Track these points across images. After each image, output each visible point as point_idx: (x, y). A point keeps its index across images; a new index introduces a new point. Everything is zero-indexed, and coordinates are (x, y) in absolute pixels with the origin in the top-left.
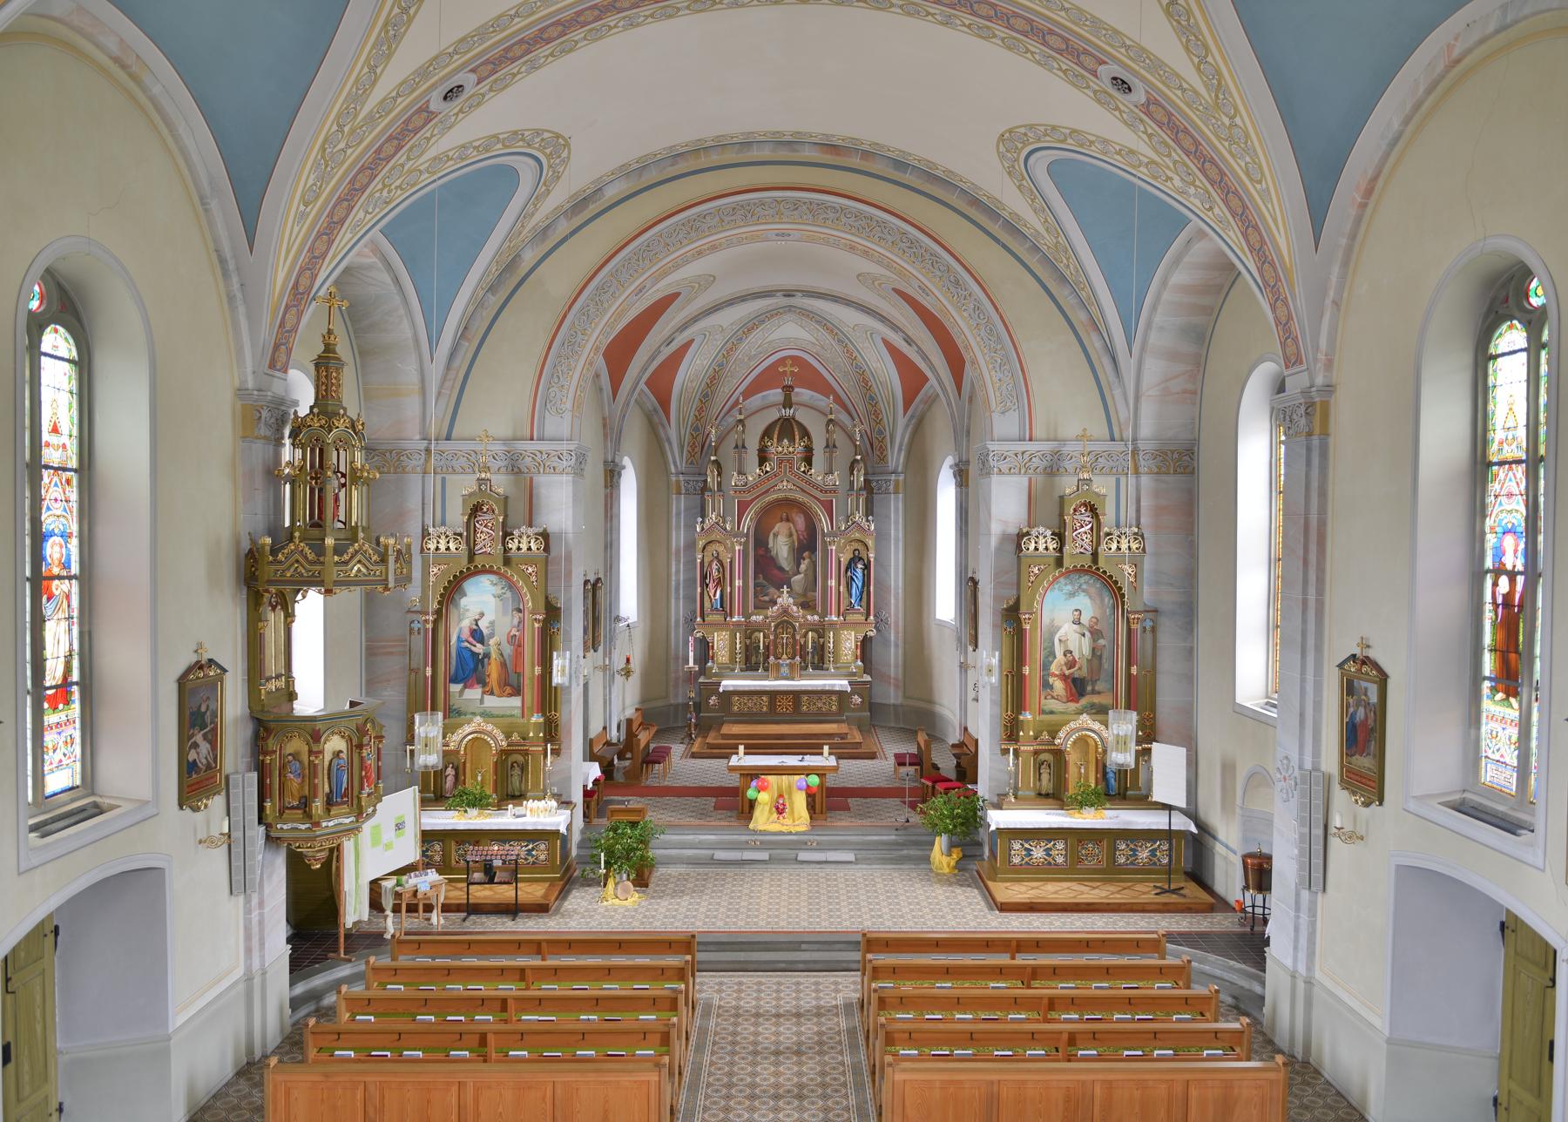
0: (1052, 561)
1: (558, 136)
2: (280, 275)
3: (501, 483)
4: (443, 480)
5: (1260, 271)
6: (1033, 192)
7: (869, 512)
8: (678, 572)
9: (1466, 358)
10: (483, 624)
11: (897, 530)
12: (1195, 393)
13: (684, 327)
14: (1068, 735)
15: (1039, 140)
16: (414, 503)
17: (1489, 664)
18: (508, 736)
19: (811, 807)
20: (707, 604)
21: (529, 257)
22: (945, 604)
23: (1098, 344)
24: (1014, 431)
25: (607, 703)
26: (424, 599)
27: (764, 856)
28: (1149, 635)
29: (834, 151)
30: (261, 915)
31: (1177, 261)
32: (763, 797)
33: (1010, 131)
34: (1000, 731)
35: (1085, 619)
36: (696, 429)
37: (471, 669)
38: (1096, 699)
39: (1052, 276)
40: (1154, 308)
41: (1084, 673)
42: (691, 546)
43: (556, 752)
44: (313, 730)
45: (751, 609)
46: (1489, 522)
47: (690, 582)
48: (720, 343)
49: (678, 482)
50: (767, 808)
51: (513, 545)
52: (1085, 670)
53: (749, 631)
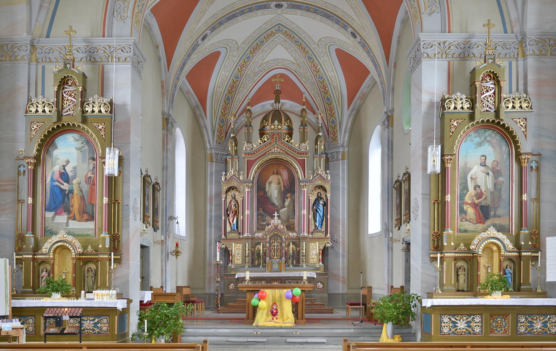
0: (466, 116)
3: (82, 67)
4: (43, 68)
7: (327, 168)
8: (211, 210)
10: (69, 169)
11: (343, 183)
16: (22, 82)
18: (85, 247)
19: (295, 312)
20: (228, 229)
24: (438, 27)
27: (264, 340)
28: (534, 173)
32: (263, 304)
36: (222, 121)
37: (60, 201)
38: (497, 221)
41: (489, 202)
42: (218, 195)
43: (118, 261)
49: (211, 154)
50: (265, 312)
51: (89, 109)
52: (489, 199)
53: (255, 242)
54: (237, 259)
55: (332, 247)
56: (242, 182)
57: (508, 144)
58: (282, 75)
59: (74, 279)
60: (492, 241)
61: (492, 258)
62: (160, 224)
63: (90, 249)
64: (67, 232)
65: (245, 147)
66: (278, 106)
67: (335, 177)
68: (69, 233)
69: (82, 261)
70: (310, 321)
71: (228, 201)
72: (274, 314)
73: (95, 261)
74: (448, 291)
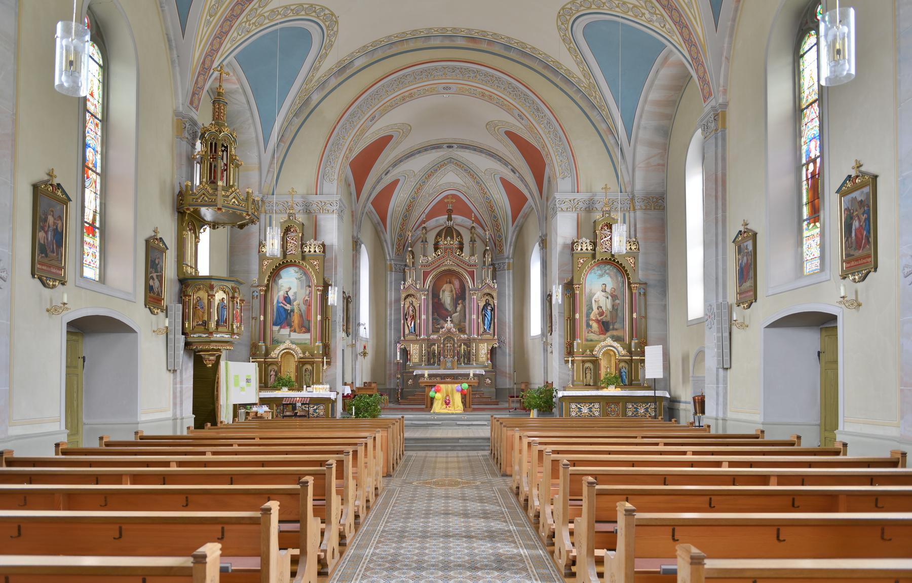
0: (590, 256)
1: (333, 14)
2: (197, 54)
3: (300, 218)
5: (690, 52)
6: (575, 51)
7: (494, 277)
9: (789, 59)
10: (291, 294)
12: (663, 165)
13: (395, 165)
14: (601, 349)
15: (578, 11)
17: (806, 212)
18: (304, 353)
20: (407, 331)
21: (316, 98)
22: (535, 326)
23: (613, 141)
24: (569, 188)
25: (354, 369)
26: (260, 279)
28: (642, 297)
29: (475, 40)
30: (181, 388)
31: (651, 86)
32: (438, 396)
33: (563, 8)
34: (564, 351)
35: (608, 289)
36: (400, 236)
37: (284, 318)
38: (615, 333)
39: (589, 106)
40: (641, 116)
41: (608, 319)
42: (398, 301)
43: (329, 363)
44: (208, 283)
45: (431, 331)
46: (803, 140)
47: (398, 321)
48: (413, 184)
51: (306, 249)
53: (430, 343)
54: (415, 357)
55: (499, 347)
56: (419, 290)
57: (623, 276)
58: (454, 196)
59: (297, 377)
60: (609, 349)
61: (610, 361)
62: (351, 330)
63: (307, 354)
64: (290, 342)
65: (421, 260)
66: (450, 223)
67: (501, 285)
68: (293, 343)
69: (302, 363)
70: (475, 410)
71: (406, 306)
72: (447, 404)
73: (312, 363)
74: (578, 385)
